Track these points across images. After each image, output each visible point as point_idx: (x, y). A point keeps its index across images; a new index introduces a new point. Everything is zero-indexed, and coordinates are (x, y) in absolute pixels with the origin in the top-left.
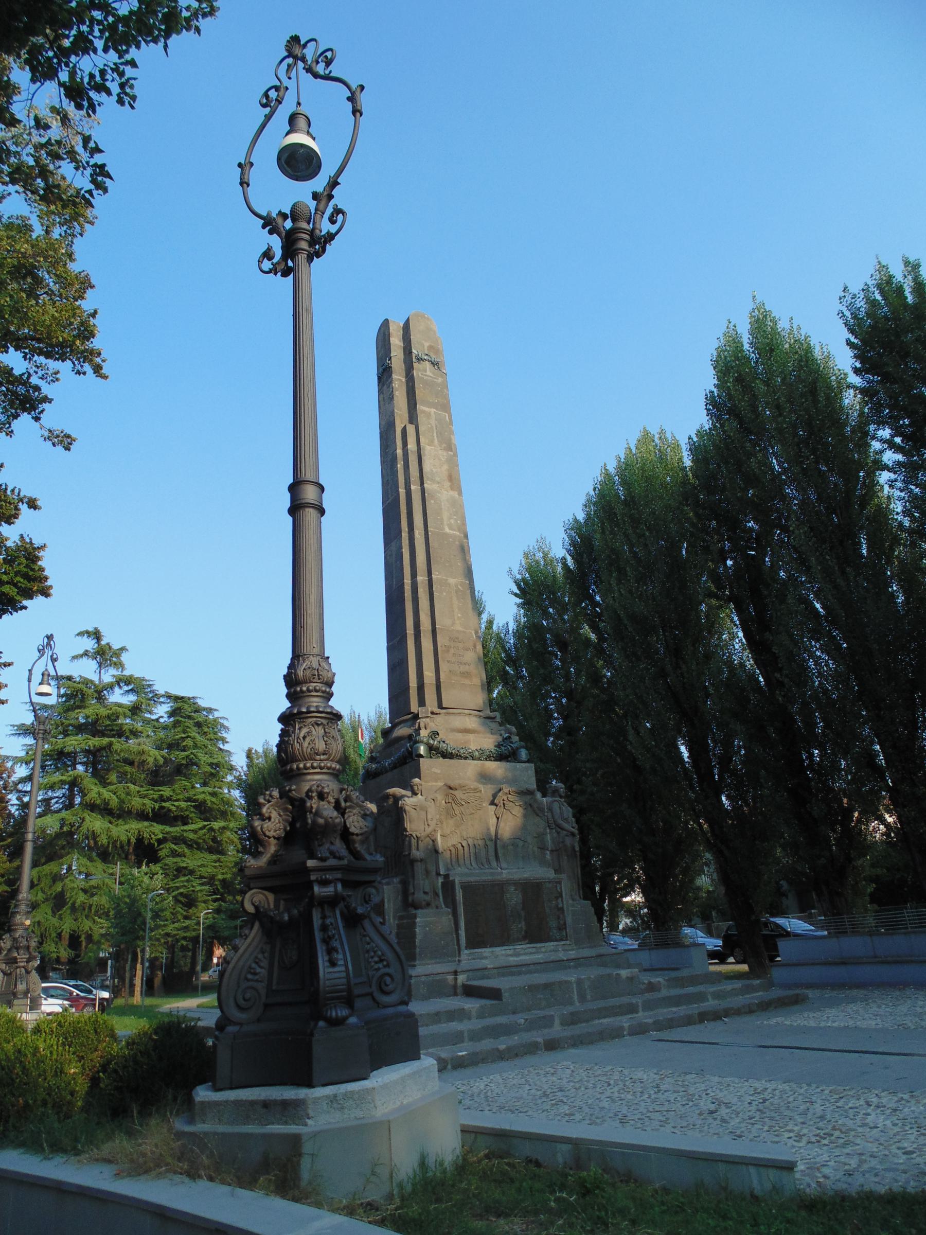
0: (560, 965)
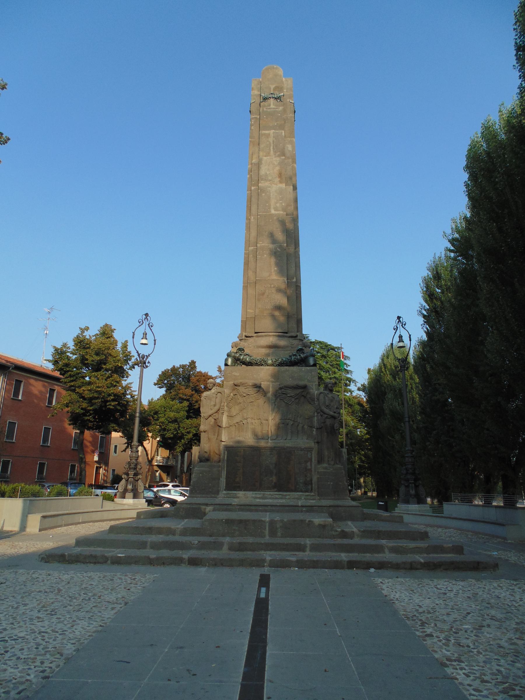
0: (265, 508)
